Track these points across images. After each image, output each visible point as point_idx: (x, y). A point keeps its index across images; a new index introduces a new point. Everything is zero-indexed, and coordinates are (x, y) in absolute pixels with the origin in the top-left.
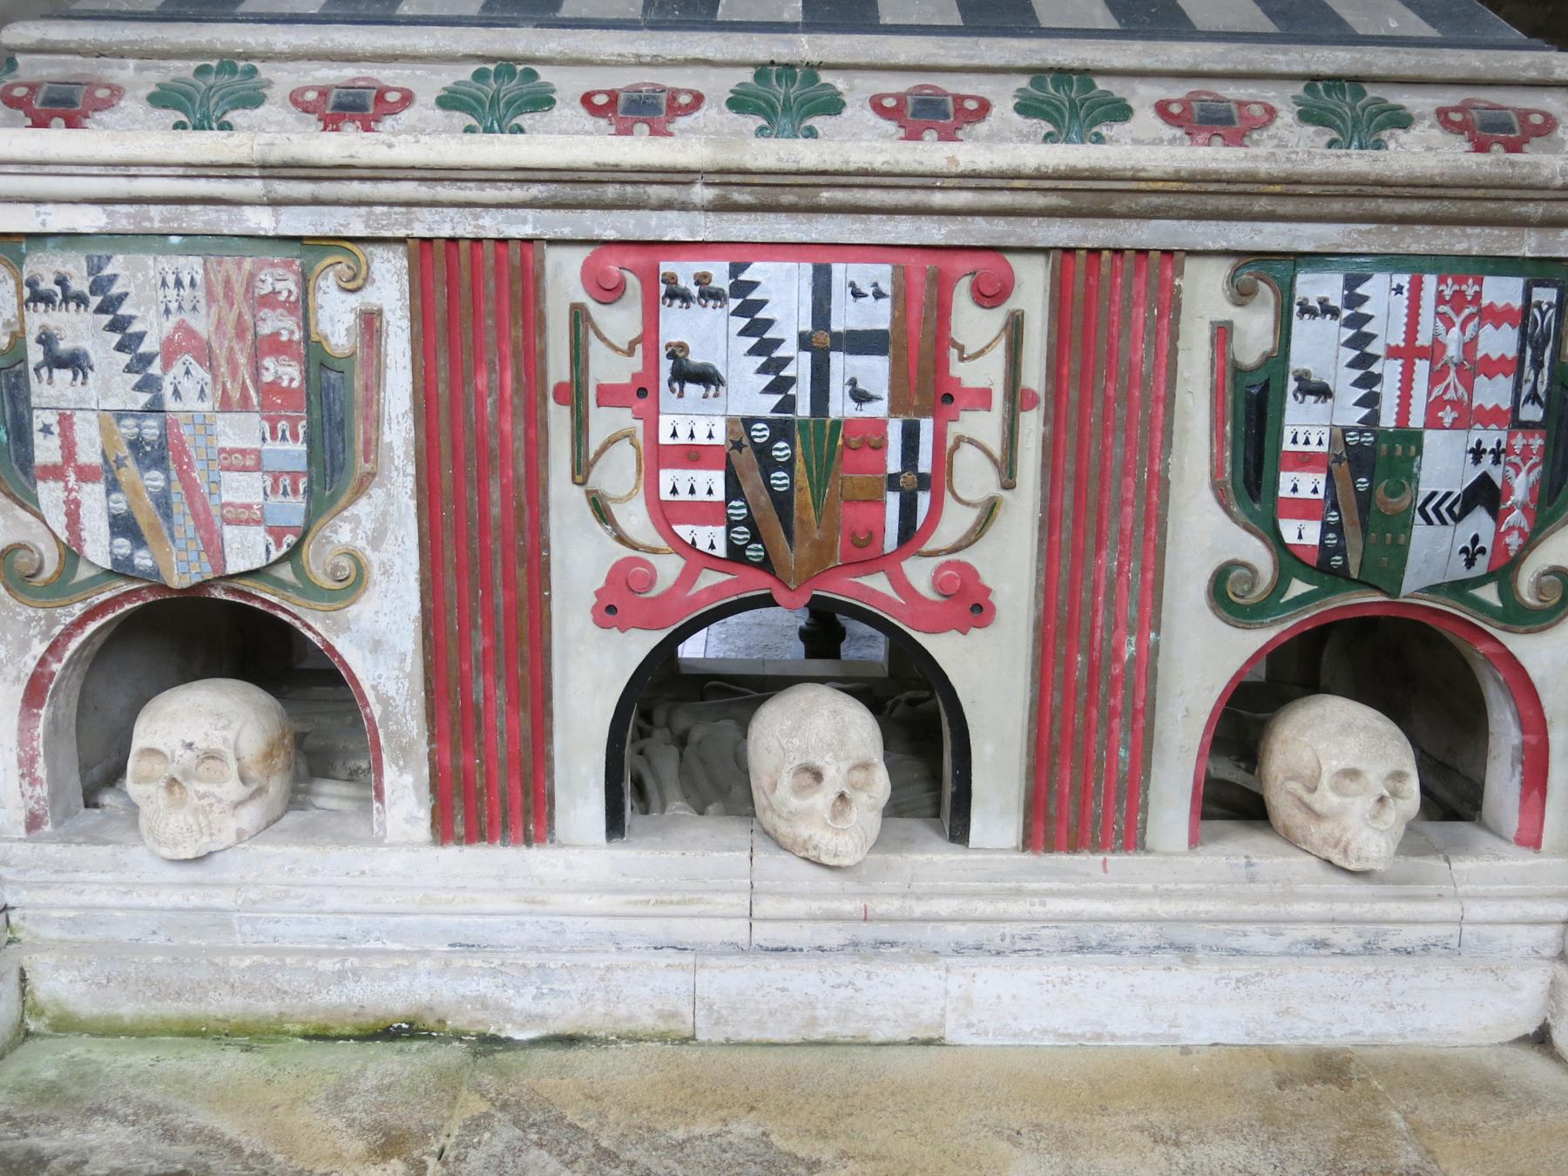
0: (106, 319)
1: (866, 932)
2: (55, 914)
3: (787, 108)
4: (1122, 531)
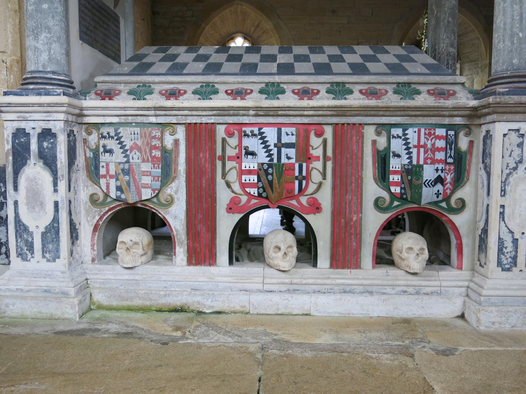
0: (118, 142)
1: (292, 287)
2: (98, 281)
3: (272, 93)
4: (352, 189)
